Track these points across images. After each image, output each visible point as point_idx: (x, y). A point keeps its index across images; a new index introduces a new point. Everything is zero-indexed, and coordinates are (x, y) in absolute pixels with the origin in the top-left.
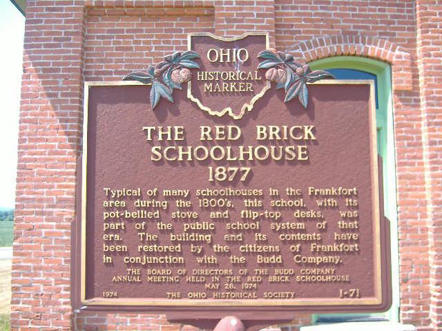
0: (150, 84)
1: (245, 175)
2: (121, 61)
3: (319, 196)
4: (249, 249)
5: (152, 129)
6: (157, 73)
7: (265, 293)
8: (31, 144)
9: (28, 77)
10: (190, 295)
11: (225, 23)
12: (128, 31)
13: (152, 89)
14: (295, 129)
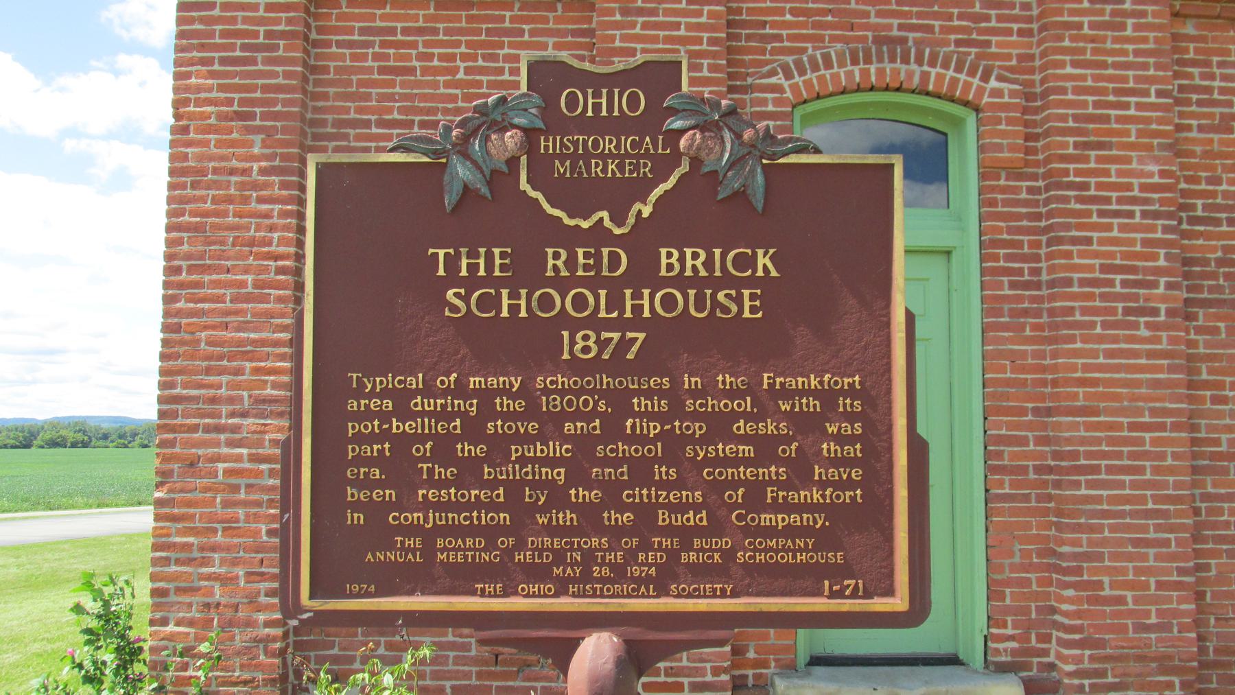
0: (444, 160)
1: (635, 348)
2: (391, 97)
3: (787, 393)
4: (641, 496)
5: (446, 254)
6: (457, 138)
7: (672, 587)
8: (194, 277)
9: (185, 130)
10: (523, 589)
11: (618, 17)
12: (405, 31)
13: (448, 171)
14: (737, 255)
